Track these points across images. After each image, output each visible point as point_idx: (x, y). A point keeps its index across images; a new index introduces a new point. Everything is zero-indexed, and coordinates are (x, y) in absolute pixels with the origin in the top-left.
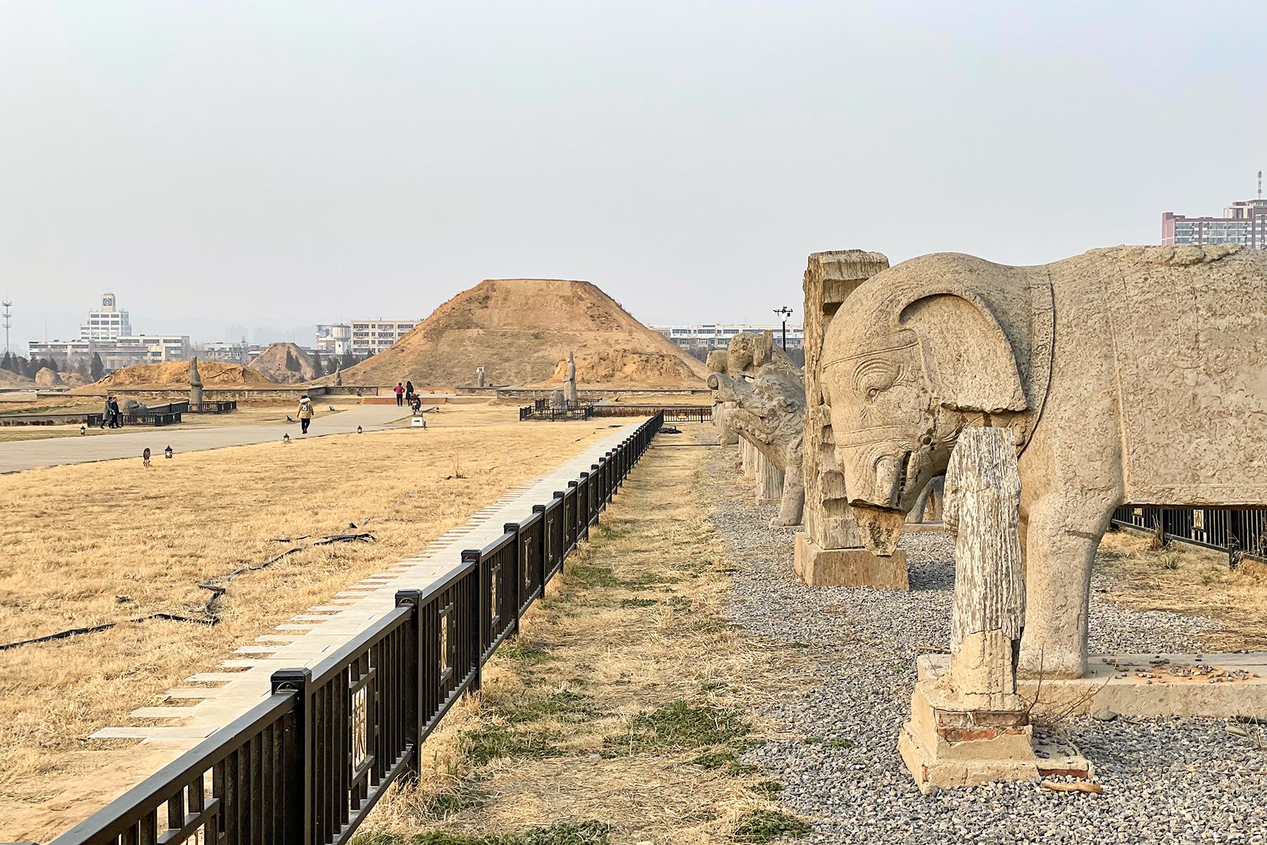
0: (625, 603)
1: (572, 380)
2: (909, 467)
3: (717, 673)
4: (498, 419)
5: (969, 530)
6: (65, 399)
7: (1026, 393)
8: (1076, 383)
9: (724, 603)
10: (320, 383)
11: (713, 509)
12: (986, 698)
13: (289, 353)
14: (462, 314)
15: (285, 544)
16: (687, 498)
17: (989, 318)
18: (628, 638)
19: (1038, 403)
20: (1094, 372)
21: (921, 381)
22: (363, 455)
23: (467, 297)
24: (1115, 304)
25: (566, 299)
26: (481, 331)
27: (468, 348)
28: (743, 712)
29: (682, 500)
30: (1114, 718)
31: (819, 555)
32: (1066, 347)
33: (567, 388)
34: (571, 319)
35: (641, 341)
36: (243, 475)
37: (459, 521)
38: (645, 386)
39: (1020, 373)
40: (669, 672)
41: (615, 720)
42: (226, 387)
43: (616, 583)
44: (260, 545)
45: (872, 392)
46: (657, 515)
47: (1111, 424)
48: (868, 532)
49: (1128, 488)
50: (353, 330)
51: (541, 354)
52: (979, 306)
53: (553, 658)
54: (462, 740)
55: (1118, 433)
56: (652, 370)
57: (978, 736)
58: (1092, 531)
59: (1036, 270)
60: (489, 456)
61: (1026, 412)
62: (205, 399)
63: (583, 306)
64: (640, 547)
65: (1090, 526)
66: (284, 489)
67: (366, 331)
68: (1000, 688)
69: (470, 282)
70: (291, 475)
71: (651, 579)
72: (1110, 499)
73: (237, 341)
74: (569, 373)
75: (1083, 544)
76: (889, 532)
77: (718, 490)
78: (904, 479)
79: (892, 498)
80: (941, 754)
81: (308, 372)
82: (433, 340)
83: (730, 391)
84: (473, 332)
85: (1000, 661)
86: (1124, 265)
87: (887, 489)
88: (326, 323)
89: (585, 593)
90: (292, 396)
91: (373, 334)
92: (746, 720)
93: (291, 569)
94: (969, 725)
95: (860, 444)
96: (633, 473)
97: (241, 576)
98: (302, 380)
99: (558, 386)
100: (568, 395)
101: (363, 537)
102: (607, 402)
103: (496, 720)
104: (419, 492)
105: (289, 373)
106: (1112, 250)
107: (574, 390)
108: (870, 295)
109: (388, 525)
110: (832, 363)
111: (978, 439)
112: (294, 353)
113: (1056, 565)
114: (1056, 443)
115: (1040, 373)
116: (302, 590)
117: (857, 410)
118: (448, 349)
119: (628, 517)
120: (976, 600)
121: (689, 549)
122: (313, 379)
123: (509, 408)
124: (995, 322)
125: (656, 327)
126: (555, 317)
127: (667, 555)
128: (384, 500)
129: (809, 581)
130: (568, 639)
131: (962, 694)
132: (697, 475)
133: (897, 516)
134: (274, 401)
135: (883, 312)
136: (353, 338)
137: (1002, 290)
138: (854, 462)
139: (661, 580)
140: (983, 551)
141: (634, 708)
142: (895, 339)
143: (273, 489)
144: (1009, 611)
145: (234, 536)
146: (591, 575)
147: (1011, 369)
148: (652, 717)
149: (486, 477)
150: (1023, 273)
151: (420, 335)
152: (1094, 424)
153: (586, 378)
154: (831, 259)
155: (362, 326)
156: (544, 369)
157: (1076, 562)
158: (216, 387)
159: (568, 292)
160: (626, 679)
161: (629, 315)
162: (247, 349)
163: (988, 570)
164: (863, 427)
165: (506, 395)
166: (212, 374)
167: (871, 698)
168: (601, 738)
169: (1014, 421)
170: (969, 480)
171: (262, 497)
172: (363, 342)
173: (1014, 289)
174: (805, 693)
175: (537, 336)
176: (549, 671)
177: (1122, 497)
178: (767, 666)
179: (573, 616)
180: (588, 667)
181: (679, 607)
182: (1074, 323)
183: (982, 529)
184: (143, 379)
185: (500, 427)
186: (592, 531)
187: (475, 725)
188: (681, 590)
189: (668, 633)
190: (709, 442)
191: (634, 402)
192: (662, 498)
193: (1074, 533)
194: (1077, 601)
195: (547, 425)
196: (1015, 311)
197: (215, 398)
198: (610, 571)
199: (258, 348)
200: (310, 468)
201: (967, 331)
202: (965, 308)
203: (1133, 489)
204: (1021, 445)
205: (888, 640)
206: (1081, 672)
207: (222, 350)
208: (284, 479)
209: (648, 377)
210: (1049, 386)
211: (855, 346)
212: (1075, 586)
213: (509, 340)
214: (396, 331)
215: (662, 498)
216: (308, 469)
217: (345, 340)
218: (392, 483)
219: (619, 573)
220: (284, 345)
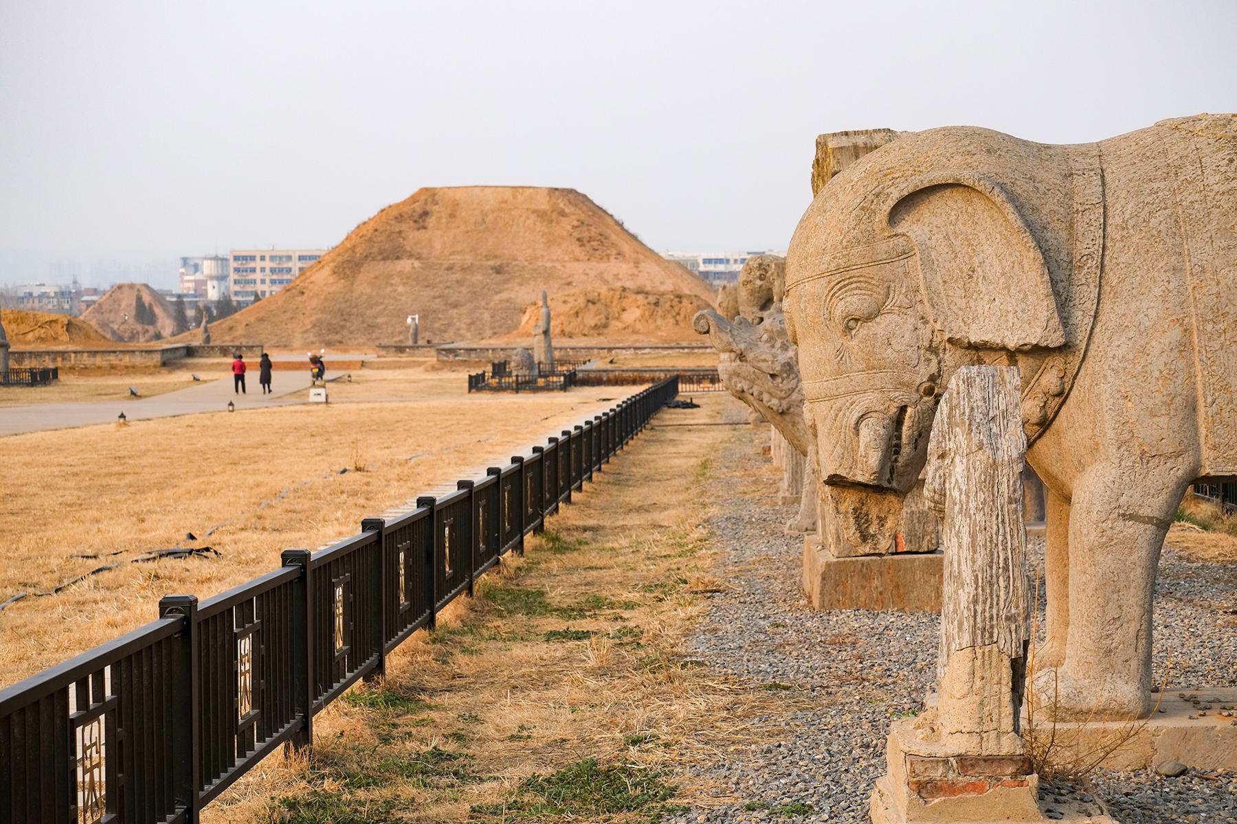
0: (551, 636)
1: (546, 332)
2: (905, 428)
3: (650, 723)
4: (437, 391)
5: (957, 508)
7: (1065, 321)
8: (1133, 306)
9: (688, 633)
10: (180, 342)
11: (713, 511)
12: (976, 739)
13: (139, 299)
14: (389, 238)
15: (90, 561)
16: (681, 497)
17: (1013, 217)
18: (544, 679)
19: (1081, 338)
20: (1157, 291)
21: (919, 307)
22: (228, 442)
23: (395, 213)
24: (1189, 196)
25: (541, 215)
26: (417, 264)
27: (398, 291)
28: (671, 772)
29: (674, 499)
30: (1184, 772)
31: (828, 565)
32: (1119, 256)
33: (537, 345)
34: (550, 243)
35: (652, 276)
36: (49, 470)
37: (344, 529)
38: (653, 341)
39: (1057, 294)
40: (587, 724)
41: (494, 784)
42: (43, 347)
43: (547, 609)
44: (54, 562)
45: (851, 323)
46: (634, 520)
47: (1181, 364)
48: (852, 520)
49: (1206, 453)
50: (233, 264)
51: (505, 295)
52: (998, 200)
53: (430, 708)
54: (273, 809)
55: (1191, 376)
56: (664, 317)
57: (964, 789)
58: (1156, 514)
59: (1083, 151)
60: (410, 441)
61: (1065, 348)
62: (13, 364)
63: (566, 225)
64: (596, 563)
65: (1155, 506)
66: (104, 489)
67: (252, 265)
68: (995, 725)
69: (399, 192)
70: (118, 469)
71: (598, 603)
72: (1181, 468)
73: (65, 282)
74: (542, 325)
75: (1142, 533)
76: (882, 521)
77: (730, 485)
78: (898, 446)
79: (880, 473)
80: (912, 816)
81: (166, 325)
82: (346, 277)
83: (727, 338)
84: (405, 265)
85: (996, 688)
86: (1202, 142)
87: (874, 459)
88: (194, 253)
89: (499, 622)
90: (138, 360)
91: (263, 270)
92: (673, 781)
93: (91, 595)
94: (951, 776)
95: (837, 397)
96: (613, 464)
97: (21, 604)
98: (158, 337)
99: (526, 342)
100: (539, 355)
101: (202, 552)
102: (597, 364)
103: (329, 785)
104: (295, 491)
105: (139, 327)
106: (1186, 121)
107: (550, 349)
108: (849, 187)
109: (244, 535)
110: (798, 283)
111: (969, 382)
112: (147, 299)
113: (1106, 561)
114: (1106, 391)
115: (1085, 294)
116: (99, 619)
117: (830, 349)
118: (368, 290)
119: (591, 522)
120: (964, 604)
121: (664, 565)
122: (173, 335)
123: (454, 375)
124: (1020, 223)
125: (678, 254)
127: (630, 574)
128: (242, 502)
129: (816, 603)
130: (457, 682)
131: (945, 732)
132: (704, 465)
133: (892, 498)
134: (113, 367)
135: (866, 210)
136: (233, 276)
137: (1033, 179)
138: (828, 423)
139: (612, 605)
140: (973, 536)
141: (527, 770)
142: (883, 247)
143: (88, 488)
144: (1008, 618)
145: (23, 550)
146: (513, 600)
147: (1044, 288)
148: (548, 781)
149: (398, 470)
150: (1065, 154)
152: (1158, 365)
153: (568, 329)
154: (845, 142)
155: (245, 258)
156: (509, 317)
157: (1135, 557)
158: (29, 348)
159: (543, 204)
160: (525, 733)
161: (634, 238)
162: (79, 293)
163: (979, 562)
164: (839, 373)
165: (450, 356)
167: (857, 752)
168: (467, 807)
169: (1049, 361)
170: (959, 440)
171: (69, 499)
172: (248, 282)
173: (1050, 176)
174: (765, 747)
175: (498, 270)
176: (421, 723)
177: (1198, 465)
178: (725, 714)
179: (472, 653)
180: (476, 719)
181: (625, 640)
182: (1131, 223)
183: (972, 505)
185: (436, 403)
186: (530, 540)
187: (300, 790)
188: (634, 618)
189: (600, 672)
190: (735, 419)
191: (638, 365)
192: (645, 498)
193: (1132, 517)
194: (1136, 612)
195: (508, 399)
196: (1050, 207)
197: (27, 364)
198: (541, 594)
199: (95, 292)
200: (149, 459)
201: (982, 236)
202: (980, 205)
203: (1212, 454)
204: (1059, 395)
205: (906, 678)
206: (1140, 710)
207: (43, 296)
208: (110, 475)
209: (658, 328)
210: (1097, 312)
211: (827, 258)
212: (1133, 590)
213: (458, 276)
214: (296, 265)
215: (645, 498)
216: (144, 461)
217: (222, 278)
218: (259, 478)
219: (556, 596)
220: (131, 286)
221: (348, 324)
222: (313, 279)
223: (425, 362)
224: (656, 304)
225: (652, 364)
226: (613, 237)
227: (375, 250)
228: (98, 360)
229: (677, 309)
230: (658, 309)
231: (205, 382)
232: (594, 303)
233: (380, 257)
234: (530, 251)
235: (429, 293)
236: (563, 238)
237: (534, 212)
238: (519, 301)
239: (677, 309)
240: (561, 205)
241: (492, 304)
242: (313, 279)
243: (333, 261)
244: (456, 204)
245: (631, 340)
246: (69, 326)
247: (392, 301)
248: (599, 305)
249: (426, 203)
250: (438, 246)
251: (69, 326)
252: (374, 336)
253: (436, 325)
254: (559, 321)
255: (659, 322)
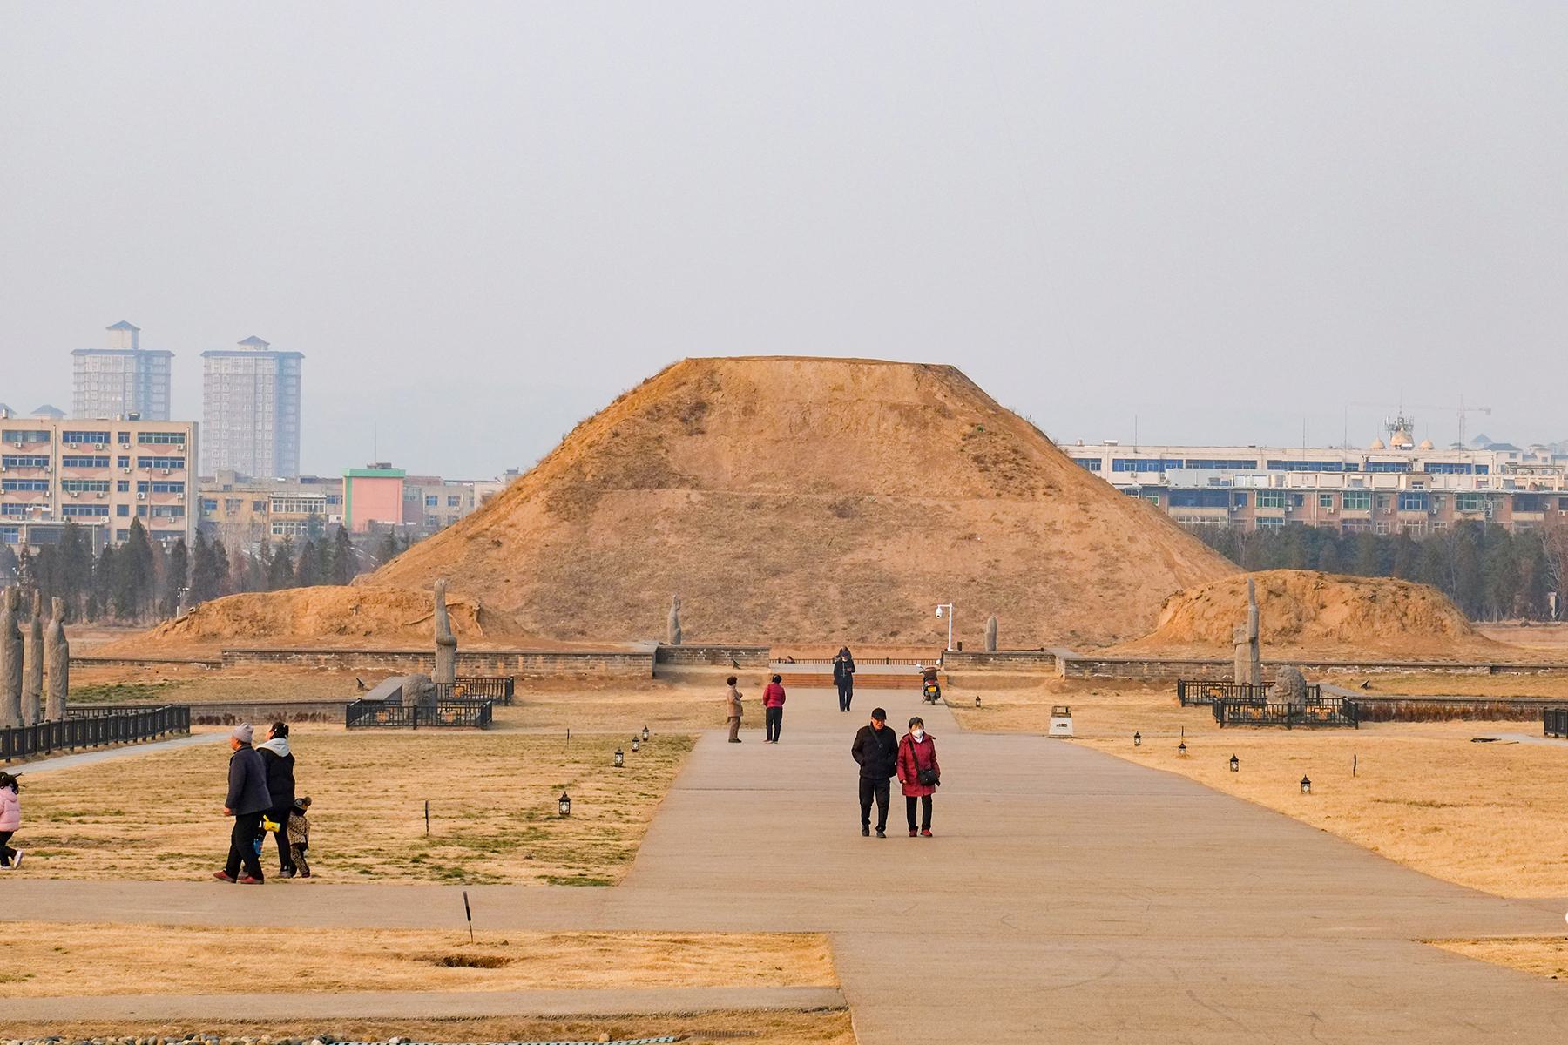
1: (1253, 641)
6: (128, 668)
14: (641, 450)
23: (647, 403)
25: (907, 414)
26: (695, 496)
27: (662, 538)
34: (926, 464)
51: (859, 556)
56: (1384, 618)
63: (953, 432)
84: (675, 498)
90: (618, 668)
107: (1257, 663)
126: (882, 463)
134: (580, 678)
151: (535, 507)
155: (88, 437)
166: (411, 616)
175: (841, 511)
184: (267, 628)
209: (1376, 635)
213: (771, 519)
221: (590, 602)
222: (512, 519)
223: (1043, 679)
224: (1373, 599)
225: (1402, 689)
226: (1037, 456)
227: (619, 469)
228: (559, 667)
229: (1402, 607)
230: (1377, 606)
231: (533, 704)
232: (1279, 596)
233: (628, 483)
234: (892, 478)
235: (724, 548)
236: (949, 456)
237: (893, 407)
238: (886, 565)
239: (1402, 607)
240: (939, 397)
241: (839, 570)
242: (512, 519)
243: (546, 487)
244: (753, 391)
245: (1342, 653)
246: (481, 614)
247: (662, 562)
248: (1285, 599)
249: (699, 388)
250: (727, 465)
251: (481, 614)
252: (640, 623)
253: (746, 606)
254: (1226, 621)
255: (1377, 626)
